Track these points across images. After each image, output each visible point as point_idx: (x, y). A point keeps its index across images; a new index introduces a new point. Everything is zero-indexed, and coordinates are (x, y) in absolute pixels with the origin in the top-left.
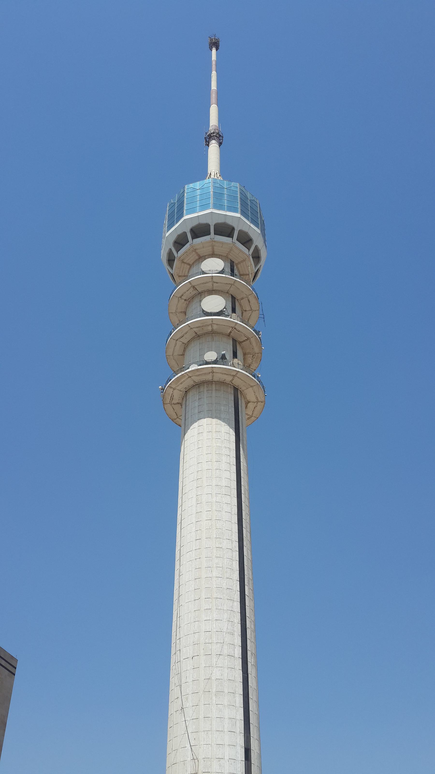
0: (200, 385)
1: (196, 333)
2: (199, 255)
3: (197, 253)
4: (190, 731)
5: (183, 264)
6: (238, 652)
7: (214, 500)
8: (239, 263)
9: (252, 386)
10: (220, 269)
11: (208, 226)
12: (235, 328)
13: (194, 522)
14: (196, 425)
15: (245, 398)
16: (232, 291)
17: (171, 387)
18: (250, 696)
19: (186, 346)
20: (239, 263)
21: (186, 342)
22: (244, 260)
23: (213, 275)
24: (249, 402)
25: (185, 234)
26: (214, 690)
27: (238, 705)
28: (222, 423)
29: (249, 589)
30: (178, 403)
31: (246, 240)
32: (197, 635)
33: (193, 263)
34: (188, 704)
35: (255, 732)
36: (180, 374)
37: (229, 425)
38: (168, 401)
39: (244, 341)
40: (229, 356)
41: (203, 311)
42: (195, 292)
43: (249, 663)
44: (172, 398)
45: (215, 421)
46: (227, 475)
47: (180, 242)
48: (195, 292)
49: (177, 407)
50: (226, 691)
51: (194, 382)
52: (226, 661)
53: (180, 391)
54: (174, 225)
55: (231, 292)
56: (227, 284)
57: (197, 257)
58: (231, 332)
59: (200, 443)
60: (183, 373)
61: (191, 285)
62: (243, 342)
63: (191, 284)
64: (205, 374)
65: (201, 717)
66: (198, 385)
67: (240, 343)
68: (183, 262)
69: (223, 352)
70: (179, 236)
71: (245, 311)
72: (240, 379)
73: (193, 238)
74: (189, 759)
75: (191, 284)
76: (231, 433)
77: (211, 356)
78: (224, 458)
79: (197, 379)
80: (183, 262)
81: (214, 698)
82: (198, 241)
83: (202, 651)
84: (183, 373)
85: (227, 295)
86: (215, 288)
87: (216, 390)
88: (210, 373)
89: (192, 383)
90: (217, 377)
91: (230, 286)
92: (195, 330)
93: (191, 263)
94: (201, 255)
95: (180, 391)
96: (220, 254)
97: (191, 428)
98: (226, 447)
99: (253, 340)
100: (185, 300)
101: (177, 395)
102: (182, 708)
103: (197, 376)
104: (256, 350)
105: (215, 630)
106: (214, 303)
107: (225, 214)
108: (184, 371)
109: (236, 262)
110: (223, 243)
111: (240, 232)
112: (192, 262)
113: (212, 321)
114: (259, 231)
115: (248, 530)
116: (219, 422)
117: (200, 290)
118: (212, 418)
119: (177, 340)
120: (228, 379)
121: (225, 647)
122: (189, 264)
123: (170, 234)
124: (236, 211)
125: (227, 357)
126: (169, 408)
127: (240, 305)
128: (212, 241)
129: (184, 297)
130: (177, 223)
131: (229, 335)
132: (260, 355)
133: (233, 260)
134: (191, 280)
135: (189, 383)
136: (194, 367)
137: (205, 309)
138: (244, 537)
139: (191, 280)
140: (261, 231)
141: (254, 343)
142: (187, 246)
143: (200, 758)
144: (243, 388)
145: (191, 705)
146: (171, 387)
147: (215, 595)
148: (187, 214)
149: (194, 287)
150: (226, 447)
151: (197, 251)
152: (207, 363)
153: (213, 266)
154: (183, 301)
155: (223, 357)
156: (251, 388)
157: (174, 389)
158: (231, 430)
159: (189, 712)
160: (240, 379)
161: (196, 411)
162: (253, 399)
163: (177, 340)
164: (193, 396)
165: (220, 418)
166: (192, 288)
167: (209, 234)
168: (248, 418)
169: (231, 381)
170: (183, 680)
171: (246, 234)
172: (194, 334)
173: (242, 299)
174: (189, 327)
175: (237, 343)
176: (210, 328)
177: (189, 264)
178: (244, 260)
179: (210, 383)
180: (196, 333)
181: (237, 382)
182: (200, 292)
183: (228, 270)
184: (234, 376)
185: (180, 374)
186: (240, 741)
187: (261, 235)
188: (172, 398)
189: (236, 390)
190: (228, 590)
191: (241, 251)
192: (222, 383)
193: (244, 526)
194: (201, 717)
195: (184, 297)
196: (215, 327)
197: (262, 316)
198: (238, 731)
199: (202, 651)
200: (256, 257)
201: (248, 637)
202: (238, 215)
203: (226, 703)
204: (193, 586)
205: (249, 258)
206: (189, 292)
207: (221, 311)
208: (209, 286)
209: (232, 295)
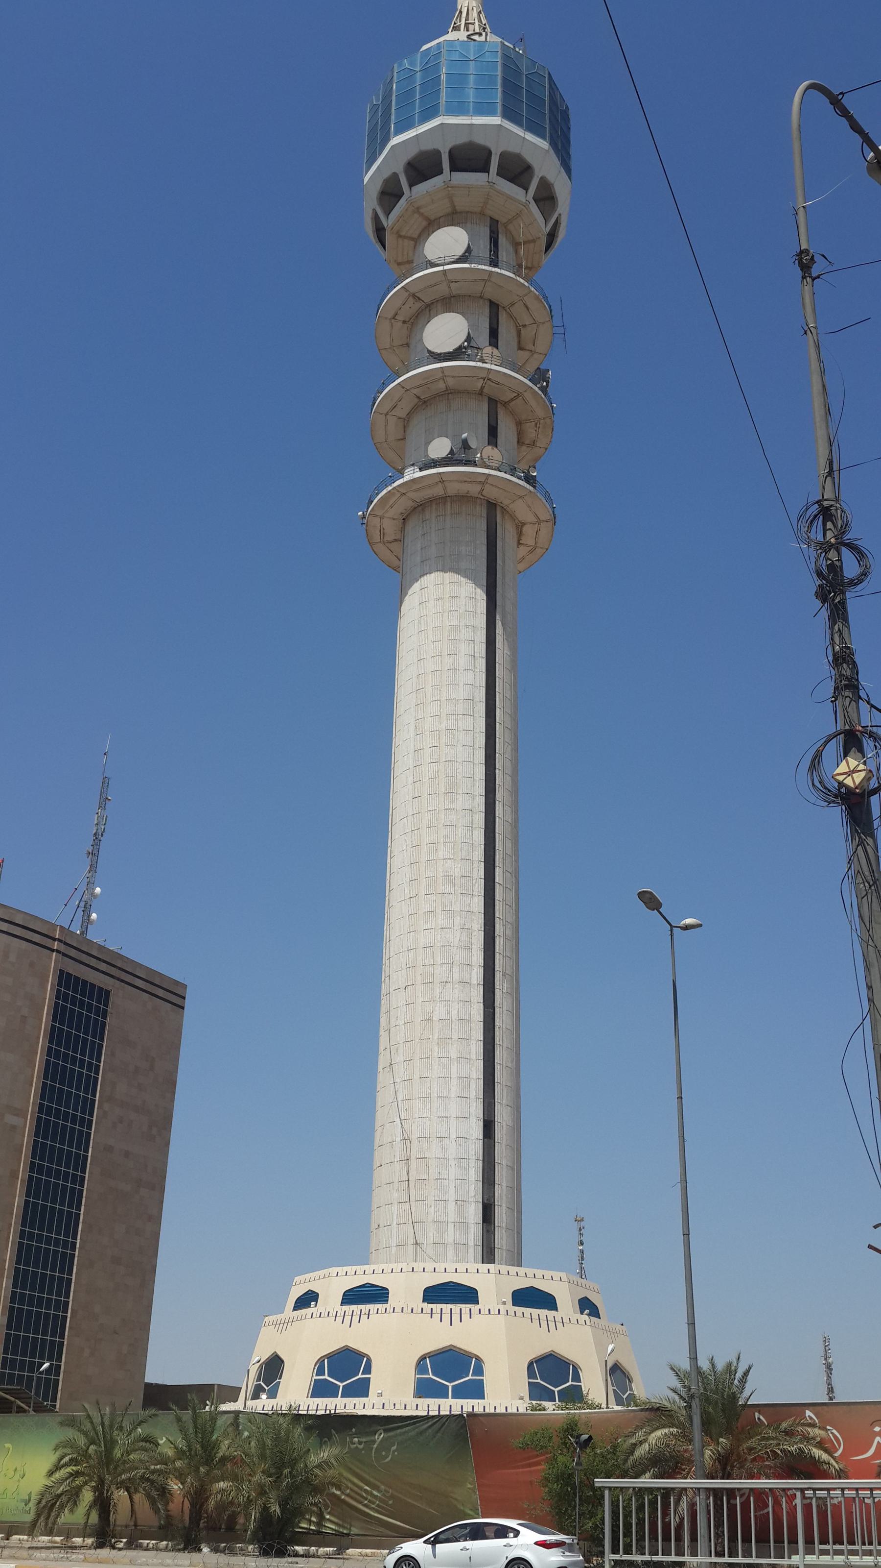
0: (424, 505)
1: (418, 397)
2: (427, 219)
3: (422, 214)
4: (400, 1098)
5: (400, 240)
6: (477, 975)
7: (443, 726)
8: (510, 221)
9: (520, 497)
10: (460, 251)
11: (437, 153)
12: (489, 379)
13: (411, 767)
14: (416, 587)
15: (513, 518)
16: (490, 292)
17: (376, 516)
18: (497, 1041)
19: (406, 422)
20: (510, 221)
21: (403, 414)
22: (518, 215)
23: (446, 267)
24: (523, 524)
25: (395, 176)
26: (436, 1037)
27: (473, 1056)
28: (462, 579)
29: (504, 872)
30: (396, 540)
31: (516, 170)
32: (412, 953)
33: (420, 235)
34: (399, 1058)
35: (505, 1094)
36: (385, 491)
37: (475, 581)
38: (377, 538)
39: (512, 400)
40: (477, 438)
41: (429, 352)
42: (419, 305)
43: (497, 991)
44: (382, 533)
45: (448, 576)
46: (468, 677)
47: (390, 194)
48: (419, 305)
49: (395, 547)
50: (455, 1036)
51: (414, 501)
52: (457, 991)
53: (394, 519)
54: (375, 160)
55: (488, 295)
56: (475, 281)
57: (424, 223)
58: (482, 388)
59: (423, 622)
60: (390, 488)
61: (407, 294)
62: (510, 401)
63: (407, 291)
64: (429, 486)
65: (416, 1077)
66: (420, 508)
67: (505, 404)
68: (400, 236)
69: (465, 435)
70: (387, 182)
71: (524, 326)
72: (496, 486)
73: (411, 185)
74: (398, 1139)
75: (407, 291)
76: (478, 597)
77: (440, 447)
78: (464, 648)
79: (419, 496)
80: (400, 236)
81: (436, 1048)
82: (422, 188)
83: (419, 978)
84: (390, 488)
85: (481, 301)
86: (454, 293)
87: (452, 514)
88: (437, 483)
89: (410, 504)
90: (453, 489)
91: (483, 283)
92: (415, 391)
93: (416, 236)
94: (432, 218)
95: (394, 519)
96: (467, 209)
97: (410, 592)
98: (467, 626)
99: (528, 396)
100: (404, 322)
101: (391, 528)
102: (391, 1065)
103: (415, 491)
104: (540, 413)
105: (439, 944)
106: (446, 331)
107: (468, 122)
108: (390, 485)
109: (503, 220)
110: (469, 188)
111: (504, 156)
112: (418, 233)
113: (443, 372)
114: (544, 144)
115: (509, 771)
116: (456, 577)
117: (427, 300)
118: (444, 570)
119: (386, 414)
120: (474, 490)
121: (456, 969)
122: (412, 239)
123: (372, 176)
124: (492, 113)
125: (473, 444)
126: (380, 548)
127: (511, 316)
128: (448, 186)
129: (400, 318)
130: (380, 154)
131: (481, 393)
132: (548, 421)
133: (496, 217)
134: (405, 283)
135: (404, 504)
136: (412, 474)
137: (430, 349)
138: (497, 786)
139: (405, 283)
140: (553, 143)
141: (533, 403)
142: (402, 201)
143: (414, 1137)
144: (506, 502)
145: (402, 1060)
146: (376, 516)
147: (441, 889)
148: (398, 132)
149: (414, 296)
150: (467, 626)
151: (422, 211)
152: (435, 463)
153: (447, 243)
154: (401, 323)
155: (465, 445)
156: (520, 500)
157: (382, 518)
158: (479, 591)
159: (400, 1071)
160: (496, 486)
161: (418, 559)
162: (531, 518)
163: (386, 414)
164: (414, 528)
165: (457, 571)
166: (411, 298)
167: (440, 172)
168: (531, 552)
169: (481, 492)
170: (393, 1023)
171: (518, 158)
172: (416, 400)
173: (512, 304)
174: (403, 387)
175: (499, 405)
176: (441, 386)
177: (412, 239)
178: (518, 215)
179: (442, 500)
180: (418, 397)
181: (491, 493)
182: (426, 305)
183: (483, 247)
184: (483, 483)
185: (385, 491)
186: (476, 1110)
187: (552, 152)
188: (382, 533)
189: (492, 507)
190: (463, 880)
191: (509, 197)
192: (464, 499)
193: (498, 765)
194: (416, 1077)
195: (400, 318)
196: (451, 382)
197: (561, 330)
198: (473, 1095)
199: (419, 978)
200: (546, 198)
201: (497, 950)
202: (496, 120)
203: (454, 1055)
204: (408, 876)
205: (528, 208)
206: (407, 306)
207: (460, 348)
208: (443, 290)
209: (490, 301)
